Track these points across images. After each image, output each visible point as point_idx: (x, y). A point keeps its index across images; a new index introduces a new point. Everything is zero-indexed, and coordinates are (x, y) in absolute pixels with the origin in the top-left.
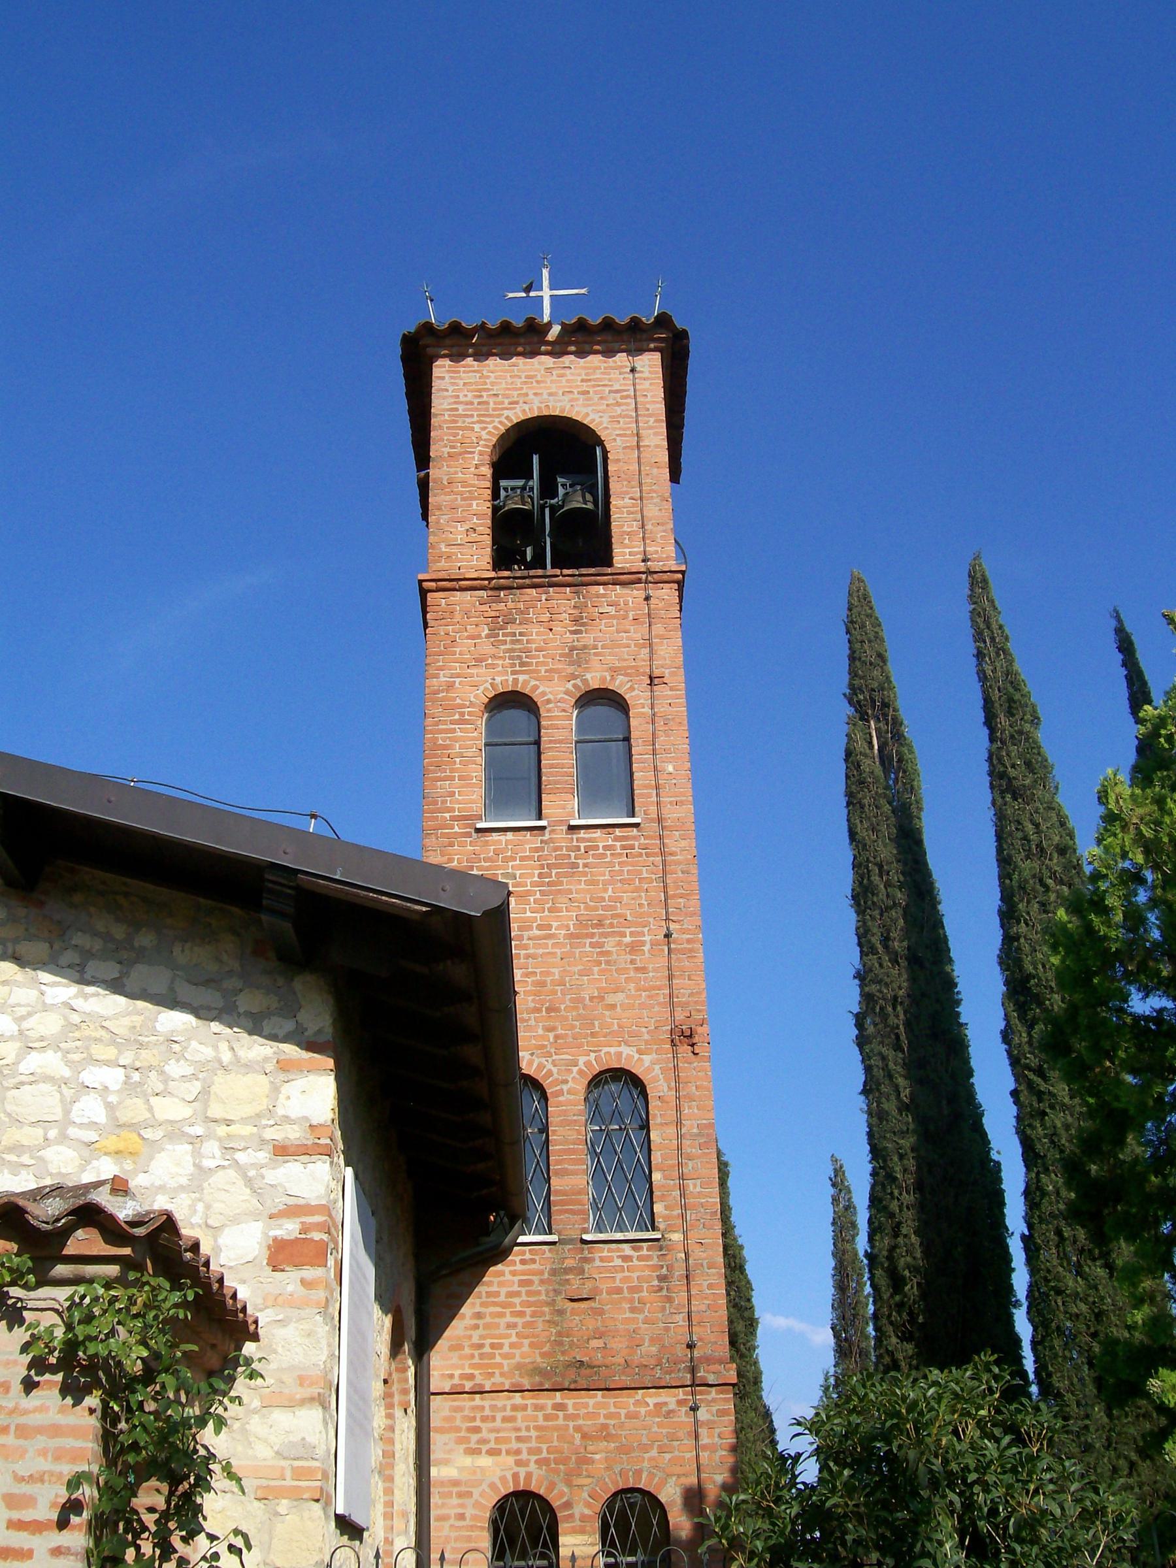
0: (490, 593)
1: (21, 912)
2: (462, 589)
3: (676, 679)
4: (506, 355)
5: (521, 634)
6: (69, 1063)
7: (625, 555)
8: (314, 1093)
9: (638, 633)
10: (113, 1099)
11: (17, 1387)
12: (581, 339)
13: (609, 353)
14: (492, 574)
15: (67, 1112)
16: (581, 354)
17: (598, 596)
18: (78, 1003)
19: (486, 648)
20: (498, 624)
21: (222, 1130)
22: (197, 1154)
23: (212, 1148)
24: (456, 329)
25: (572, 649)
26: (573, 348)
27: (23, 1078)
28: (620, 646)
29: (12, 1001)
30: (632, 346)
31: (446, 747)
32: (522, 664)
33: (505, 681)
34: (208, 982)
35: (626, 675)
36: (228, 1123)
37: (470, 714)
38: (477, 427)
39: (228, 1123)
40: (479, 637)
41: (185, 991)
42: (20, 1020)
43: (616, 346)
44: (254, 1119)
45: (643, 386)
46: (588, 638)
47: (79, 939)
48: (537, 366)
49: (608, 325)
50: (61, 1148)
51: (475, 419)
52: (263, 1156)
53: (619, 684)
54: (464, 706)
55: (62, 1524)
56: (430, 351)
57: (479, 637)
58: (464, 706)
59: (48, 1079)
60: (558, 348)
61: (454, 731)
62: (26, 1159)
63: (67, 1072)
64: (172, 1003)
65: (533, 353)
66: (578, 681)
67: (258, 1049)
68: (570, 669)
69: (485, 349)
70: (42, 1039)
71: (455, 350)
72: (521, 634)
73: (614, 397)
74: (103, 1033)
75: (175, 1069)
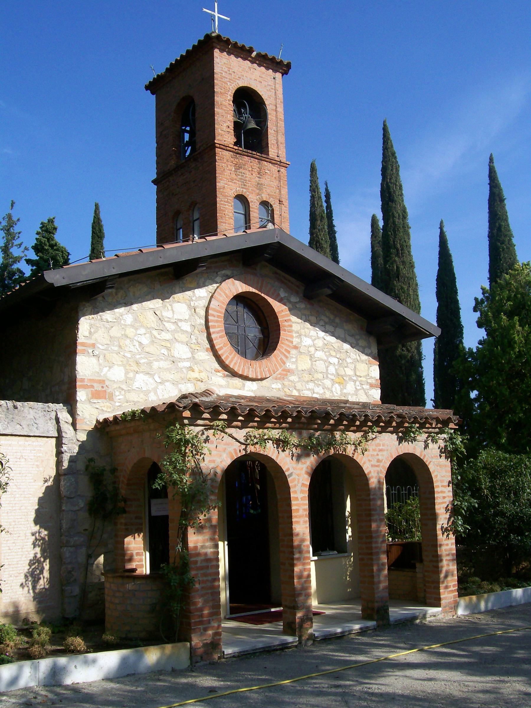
0: (235, 154)
1: (309, 306)
2: (227, 150)
3: (286, 202)
4: (237, 56)
5: (244, 173)
6: (326, 356)
7: (272, 152)
8: (375, 371)
9: (275, 183)
10: (337, 367)
11: (439, 457)
12: (262, 60)
13: (267, 68)
14: (232, 146)
15: (327, 370)
16: (260, 65)
17: (265, 166)
18: (325, 337)
19: (234, 176)
20: (238, 167)
21: (360, 379)
22: (355, 384)
23: (358, 383)
24: (228, 42)
25: (258, 184)
26: (257, 62)
27: (317, 359)
28: (272, 187)
29: (310, 334)
30: (275, 69)
31: (224, 211)
32: (245, 185)
33: (241, 191)
34: (352, 336)
35: (273, 198)
36: (361, 377)
37: (230, 200)
38: (229, 83)
39: (361, 377)
40: (232, 170)
41: (349, 338)
42: (313, 341)
43: (270, 66)
44: (365, 376)
45: (277, 86)
46: (263, 181)
47: (323, 317)
48: (246, 65)
49: (273, 60)
50: (327, 380)
51: (228, 80)
52: (368, 387)
53: (271, 201)
54: (228, 196)
55: (449, 486)
56: (215, 44)
57: (232, 170)
58: (228, 196)
59: (322, 360)
60: (253, 60)
61: (225, 205)
62: (320, 383)
63: (326, 359)
64: (345, 341)
65: (245, 59)
66: (260, 196)
67: (364, 357)
68: (258, 191)
69: (231, 51)
70: (319, 347)
71: (222, 48)
72: (244, 173)
73: (267, 85)
74: (332, 347)
75: (349, 360)
